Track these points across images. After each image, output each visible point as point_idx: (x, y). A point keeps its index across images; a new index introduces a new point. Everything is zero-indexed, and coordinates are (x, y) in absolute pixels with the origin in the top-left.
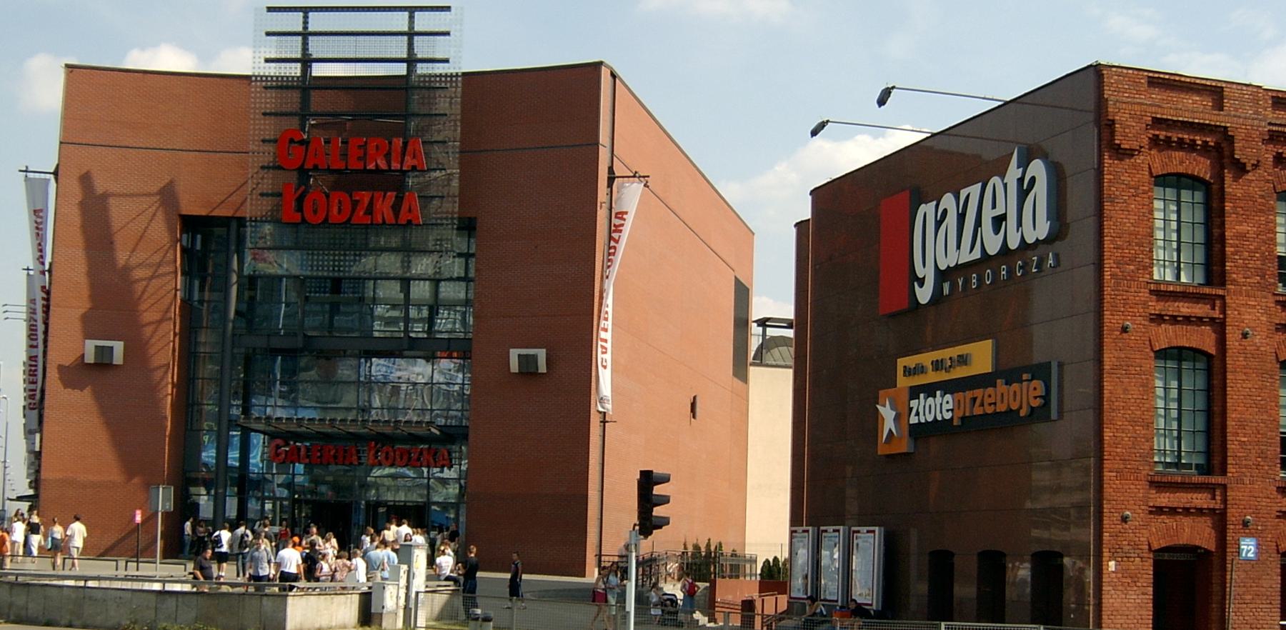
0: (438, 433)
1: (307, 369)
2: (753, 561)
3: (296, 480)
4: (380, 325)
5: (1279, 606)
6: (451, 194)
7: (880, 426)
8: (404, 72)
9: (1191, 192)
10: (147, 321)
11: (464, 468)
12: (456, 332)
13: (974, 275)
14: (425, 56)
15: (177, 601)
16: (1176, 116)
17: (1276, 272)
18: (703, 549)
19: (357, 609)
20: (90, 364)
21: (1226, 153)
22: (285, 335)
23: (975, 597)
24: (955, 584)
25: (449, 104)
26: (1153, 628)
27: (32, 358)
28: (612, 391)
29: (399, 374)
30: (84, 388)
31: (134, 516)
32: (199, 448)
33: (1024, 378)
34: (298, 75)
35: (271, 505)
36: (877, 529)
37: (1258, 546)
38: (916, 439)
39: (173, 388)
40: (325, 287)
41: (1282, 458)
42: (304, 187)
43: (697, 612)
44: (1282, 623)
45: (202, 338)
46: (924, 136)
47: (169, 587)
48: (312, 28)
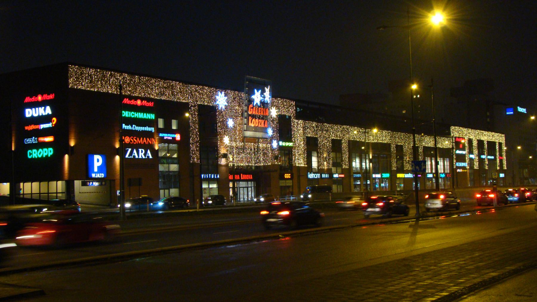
1: (413, 175)
2: (224, 143)
3: (231, 187)
5: (34, 109)
7: (90, 164)
10: (336, 190)
11: (371, 157)
15: (340, 186)
16: (321, 199)
17: (497, 141)
18: (412, 24)
19: (163, 124)
25: (173, 187)
27: (381, 223)
28: (159, 167)
29: (486, 299)
32: (415, 184)
33: (446, 182)
35: (354, 164)
36: (297, 165)
37: (25, 129)
38: (273, 97)
39: (370, 163)
42: (314, 200)
44: (291, 144)
46: (472, 284)
47: (131, 211)
48: (249, 188)
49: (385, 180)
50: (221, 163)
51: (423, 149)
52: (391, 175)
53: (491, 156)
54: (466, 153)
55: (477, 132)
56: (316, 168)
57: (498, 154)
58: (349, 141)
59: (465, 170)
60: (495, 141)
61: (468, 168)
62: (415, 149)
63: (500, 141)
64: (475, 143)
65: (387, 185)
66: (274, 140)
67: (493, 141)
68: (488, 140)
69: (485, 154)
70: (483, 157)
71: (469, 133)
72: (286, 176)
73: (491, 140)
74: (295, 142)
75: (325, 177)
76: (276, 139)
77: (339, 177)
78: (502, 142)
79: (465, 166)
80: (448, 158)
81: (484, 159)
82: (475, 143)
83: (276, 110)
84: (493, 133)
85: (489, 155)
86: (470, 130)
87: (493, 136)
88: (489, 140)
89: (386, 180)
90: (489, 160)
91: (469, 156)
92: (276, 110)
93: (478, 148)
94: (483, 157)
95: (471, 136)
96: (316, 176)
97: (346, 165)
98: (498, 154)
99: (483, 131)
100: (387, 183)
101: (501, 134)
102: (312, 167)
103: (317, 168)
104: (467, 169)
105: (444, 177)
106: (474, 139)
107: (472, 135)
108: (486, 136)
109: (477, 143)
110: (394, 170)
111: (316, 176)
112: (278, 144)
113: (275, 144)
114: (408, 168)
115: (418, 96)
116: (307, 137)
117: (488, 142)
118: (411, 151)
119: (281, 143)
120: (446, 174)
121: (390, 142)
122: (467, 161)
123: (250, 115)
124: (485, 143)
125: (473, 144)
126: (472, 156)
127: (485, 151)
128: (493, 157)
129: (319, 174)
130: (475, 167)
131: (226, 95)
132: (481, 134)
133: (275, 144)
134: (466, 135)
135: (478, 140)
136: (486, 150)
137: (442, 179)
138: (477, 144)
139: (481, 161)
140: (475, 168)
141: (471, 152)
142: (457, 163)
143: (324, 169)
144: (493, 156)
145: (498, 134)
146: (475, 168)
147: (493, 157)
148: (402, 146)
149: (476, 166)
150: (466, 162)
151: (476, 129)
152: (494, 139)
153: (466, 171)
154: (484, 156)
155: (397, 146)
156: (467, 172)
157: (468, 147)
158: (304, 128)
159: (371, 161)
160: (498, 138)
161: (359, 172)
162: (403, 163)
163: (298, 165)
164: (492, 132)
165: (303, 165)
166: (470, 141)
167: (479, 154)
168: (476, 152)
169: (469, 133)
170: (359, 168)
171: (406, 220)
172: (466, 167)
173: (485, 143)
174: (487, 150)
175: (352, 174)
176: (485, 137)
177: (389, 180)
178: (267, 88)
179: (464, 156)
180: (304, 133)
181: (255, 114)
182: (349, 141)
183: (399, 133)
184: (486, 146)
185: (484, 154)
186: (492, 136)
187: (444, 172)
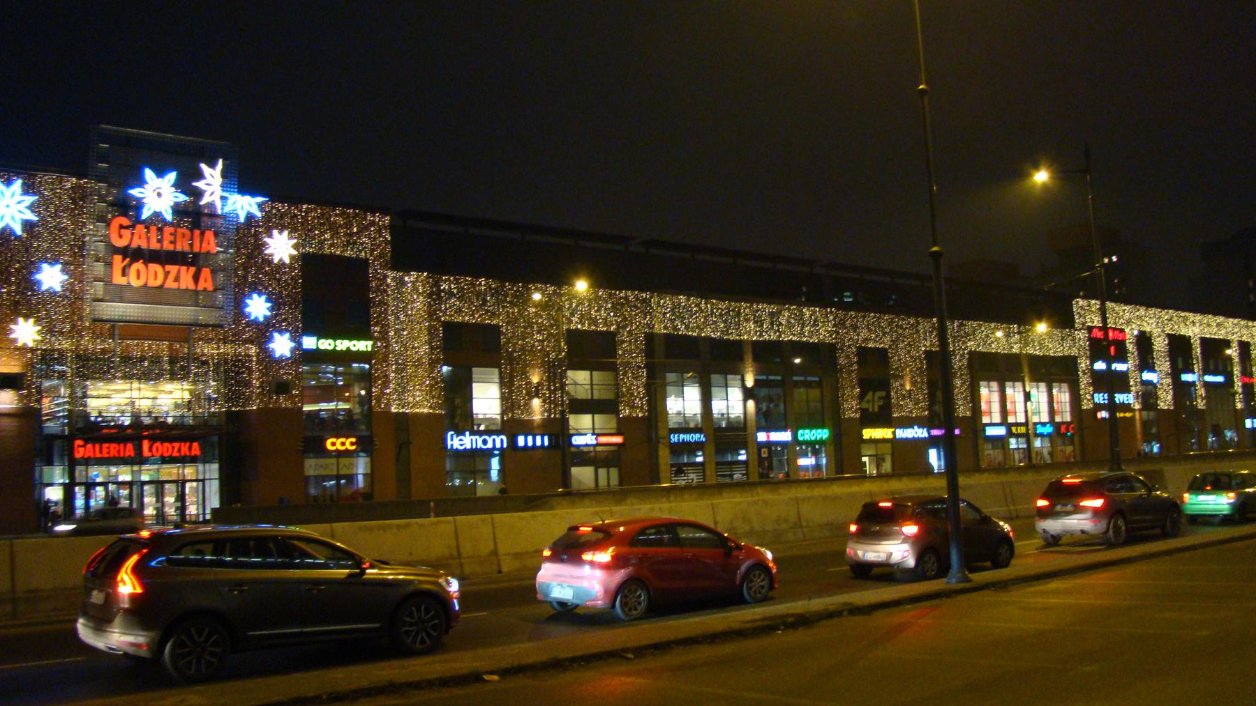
0: (889, 504)
4: (198, 367)
6: (613, 383)
8: (800, 432)
9: (723, 376)
11: (750, 382)
12: (198, 500)
13: (1114, 259)
14: (606, 481)
17: (1235, 338)
20: (504, 398)
21: (984, 482)
22: (429, 501)
23: (474, 385)
24: (161, 479)
26: (1254, 320)
30: (246, 303)
31: (1103, 419)
34: (1068, 419)
35: (673, 405)
39: (977, 411)
40: (138, 345)
41: (616, 358)
43: (1116, 395)
45: (1039, 394)
49: (804, 447)
50: (534, 418)
51: (970, 360)
52: (837, 437)
53: (1215, 373)
54: (1128, 369)
55: (1165, 315)
56: (495, 419)
57: (1237, 370)
58: (650, 338)
59: (1125, 412)
60: (1226, 338)
61: (1137, 407)
62: (938, 363)
63: (1244, 339)
64: (1160, 344)
65: (824, 461)
66: (281, 332)
67: (1221, 337)
68: (1203, 336)
69: (1196, 370)
70: (1187, 377)
71: (1139, 317)
72: (334, 444)
73: (1213, 337)
74: (384, 336)
75: (474, 447)
76: (287, 330)
77: (598, 445)
78: (1249, 340)
79: (1126, 402)
80: (993, 380)
81: (1193, 384)
82: (1160, 344)
83: (289, 239)
84: (1220, 319)
85: (1206, 371)
86: (1142, 311)
87: (1218, 325)
88: (1207, 336)
89: (807, 448)
90: (1207, 385)
91: (1141, 376)
92: (289, 239)
93: (1170, 356)
94: (1187, 377)
95: (1145, 324)
96: (485, 442)
97: (632, 407)
98: (1237, 370)
99: (1187, 314)
100: (824, 455)
101: (1245, 322)
102: (472, 414)
103: (498, 417)
104: (1133, 410)
105: (1049, 435)
106: (1156, 332)
107: (1150, 322)
108: (1197, 325)
109: (1166, 342)
110: (850, 419)
111: (485, 442)
112: (300, 344)
113: (282, 345)
114: (911, 412)
115: (1106, 260)
116: (448, 326)
117: (1204, 341)
118: (922, 363)
119: (309, 342)
120: (1057, 426)
121: (833, 339)
122: (1133, 388)
123: (117, 251)
124: (1196, 344)
125: (1152, 344)
126: (1147, 376)
127: (1195, 362)
128: (1220, 379)
129: (504, 437)
130: (1162, 404)
131: (27, 189)
132: (1181, 319)
133: (282, 345)
134: (1129, 322)
135: (1169, 336)
136: (1197, 360)
137: (1047, 440)
138: (1168, 345)
139: (1183, 391)
140: (1162, 406)
141: (1146, 362)
142: (1096, 395)
143: (531, 422)
144: (1220, 375)
145: (1236, 321)
146: (1162, 406)
147: (1220, 379)
148: (882, 355)
149: (1166, 400)
150: (1129, 393)
151: (1164, 308)
152: (1222, 332)
153: (1128, 415)
154: (1190, 375)
155: (863, 353)
156: (1133, 418)
157: (1136, 354)
158: (435, 296)
159: (748, 394)
160: (1236, 330)
161: (700, 426)
162: (888, 397)
163: (396, 411)
164: (1215, 314)
165: (425, 411)
166: (1144, 341)
167: (1175, 374)
168: (1163, 365)
169: (1139, 317)
170: (699, 416)
171: (346, 630)
172: (1130, 404)
173: (1196, 344)
174: (1200, 358)
175: (662, 433)
176: (1194, 328)
177: (832, 448)
178: (212, 165)
179: (1124, 376)
180: (431, 314)
181: (187, 249)
182: (650, 338)
183: (872, 315)
184: (1197, 350)
185: (1192, 372)
186: (1217, 326)
187: (1052, 421)
